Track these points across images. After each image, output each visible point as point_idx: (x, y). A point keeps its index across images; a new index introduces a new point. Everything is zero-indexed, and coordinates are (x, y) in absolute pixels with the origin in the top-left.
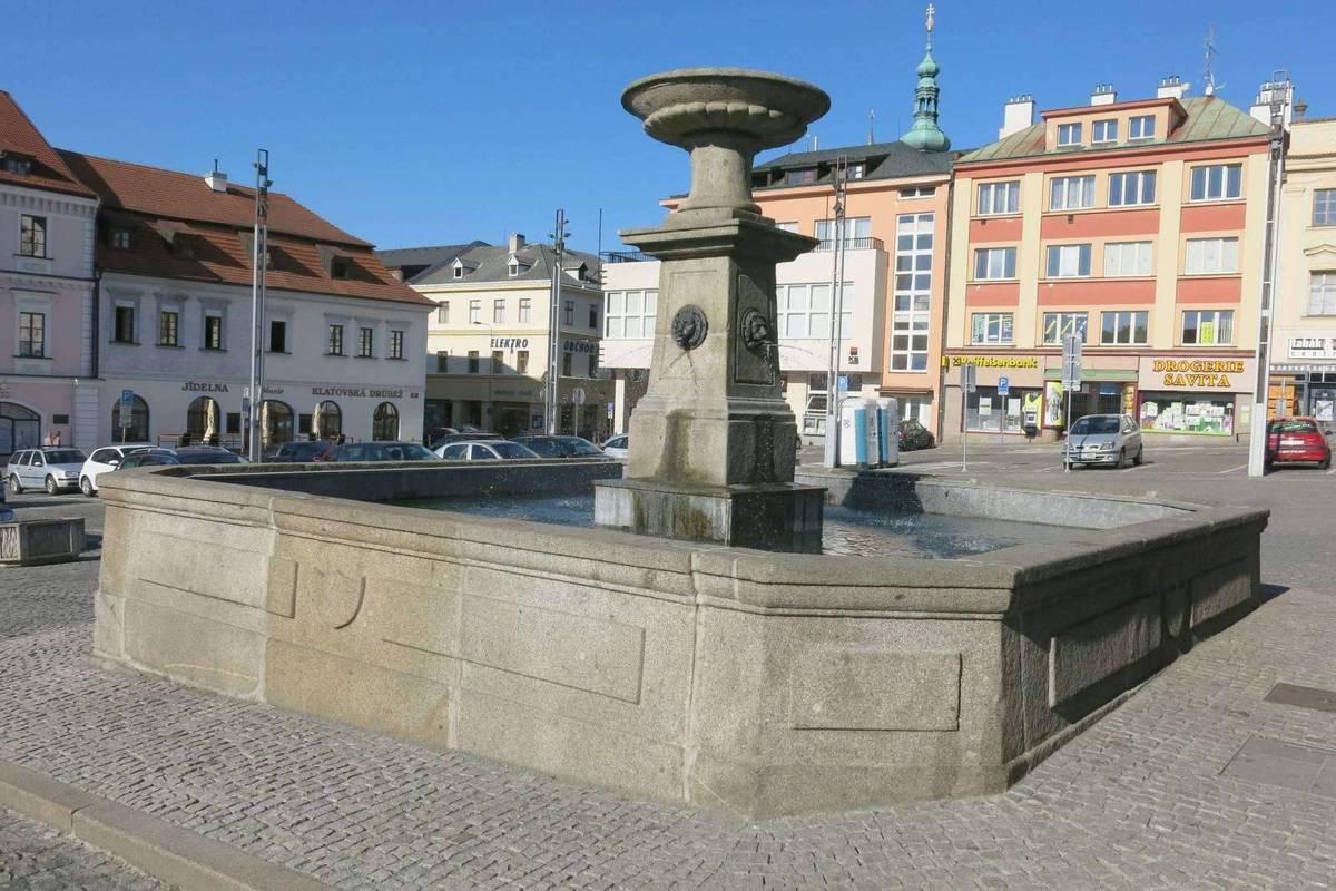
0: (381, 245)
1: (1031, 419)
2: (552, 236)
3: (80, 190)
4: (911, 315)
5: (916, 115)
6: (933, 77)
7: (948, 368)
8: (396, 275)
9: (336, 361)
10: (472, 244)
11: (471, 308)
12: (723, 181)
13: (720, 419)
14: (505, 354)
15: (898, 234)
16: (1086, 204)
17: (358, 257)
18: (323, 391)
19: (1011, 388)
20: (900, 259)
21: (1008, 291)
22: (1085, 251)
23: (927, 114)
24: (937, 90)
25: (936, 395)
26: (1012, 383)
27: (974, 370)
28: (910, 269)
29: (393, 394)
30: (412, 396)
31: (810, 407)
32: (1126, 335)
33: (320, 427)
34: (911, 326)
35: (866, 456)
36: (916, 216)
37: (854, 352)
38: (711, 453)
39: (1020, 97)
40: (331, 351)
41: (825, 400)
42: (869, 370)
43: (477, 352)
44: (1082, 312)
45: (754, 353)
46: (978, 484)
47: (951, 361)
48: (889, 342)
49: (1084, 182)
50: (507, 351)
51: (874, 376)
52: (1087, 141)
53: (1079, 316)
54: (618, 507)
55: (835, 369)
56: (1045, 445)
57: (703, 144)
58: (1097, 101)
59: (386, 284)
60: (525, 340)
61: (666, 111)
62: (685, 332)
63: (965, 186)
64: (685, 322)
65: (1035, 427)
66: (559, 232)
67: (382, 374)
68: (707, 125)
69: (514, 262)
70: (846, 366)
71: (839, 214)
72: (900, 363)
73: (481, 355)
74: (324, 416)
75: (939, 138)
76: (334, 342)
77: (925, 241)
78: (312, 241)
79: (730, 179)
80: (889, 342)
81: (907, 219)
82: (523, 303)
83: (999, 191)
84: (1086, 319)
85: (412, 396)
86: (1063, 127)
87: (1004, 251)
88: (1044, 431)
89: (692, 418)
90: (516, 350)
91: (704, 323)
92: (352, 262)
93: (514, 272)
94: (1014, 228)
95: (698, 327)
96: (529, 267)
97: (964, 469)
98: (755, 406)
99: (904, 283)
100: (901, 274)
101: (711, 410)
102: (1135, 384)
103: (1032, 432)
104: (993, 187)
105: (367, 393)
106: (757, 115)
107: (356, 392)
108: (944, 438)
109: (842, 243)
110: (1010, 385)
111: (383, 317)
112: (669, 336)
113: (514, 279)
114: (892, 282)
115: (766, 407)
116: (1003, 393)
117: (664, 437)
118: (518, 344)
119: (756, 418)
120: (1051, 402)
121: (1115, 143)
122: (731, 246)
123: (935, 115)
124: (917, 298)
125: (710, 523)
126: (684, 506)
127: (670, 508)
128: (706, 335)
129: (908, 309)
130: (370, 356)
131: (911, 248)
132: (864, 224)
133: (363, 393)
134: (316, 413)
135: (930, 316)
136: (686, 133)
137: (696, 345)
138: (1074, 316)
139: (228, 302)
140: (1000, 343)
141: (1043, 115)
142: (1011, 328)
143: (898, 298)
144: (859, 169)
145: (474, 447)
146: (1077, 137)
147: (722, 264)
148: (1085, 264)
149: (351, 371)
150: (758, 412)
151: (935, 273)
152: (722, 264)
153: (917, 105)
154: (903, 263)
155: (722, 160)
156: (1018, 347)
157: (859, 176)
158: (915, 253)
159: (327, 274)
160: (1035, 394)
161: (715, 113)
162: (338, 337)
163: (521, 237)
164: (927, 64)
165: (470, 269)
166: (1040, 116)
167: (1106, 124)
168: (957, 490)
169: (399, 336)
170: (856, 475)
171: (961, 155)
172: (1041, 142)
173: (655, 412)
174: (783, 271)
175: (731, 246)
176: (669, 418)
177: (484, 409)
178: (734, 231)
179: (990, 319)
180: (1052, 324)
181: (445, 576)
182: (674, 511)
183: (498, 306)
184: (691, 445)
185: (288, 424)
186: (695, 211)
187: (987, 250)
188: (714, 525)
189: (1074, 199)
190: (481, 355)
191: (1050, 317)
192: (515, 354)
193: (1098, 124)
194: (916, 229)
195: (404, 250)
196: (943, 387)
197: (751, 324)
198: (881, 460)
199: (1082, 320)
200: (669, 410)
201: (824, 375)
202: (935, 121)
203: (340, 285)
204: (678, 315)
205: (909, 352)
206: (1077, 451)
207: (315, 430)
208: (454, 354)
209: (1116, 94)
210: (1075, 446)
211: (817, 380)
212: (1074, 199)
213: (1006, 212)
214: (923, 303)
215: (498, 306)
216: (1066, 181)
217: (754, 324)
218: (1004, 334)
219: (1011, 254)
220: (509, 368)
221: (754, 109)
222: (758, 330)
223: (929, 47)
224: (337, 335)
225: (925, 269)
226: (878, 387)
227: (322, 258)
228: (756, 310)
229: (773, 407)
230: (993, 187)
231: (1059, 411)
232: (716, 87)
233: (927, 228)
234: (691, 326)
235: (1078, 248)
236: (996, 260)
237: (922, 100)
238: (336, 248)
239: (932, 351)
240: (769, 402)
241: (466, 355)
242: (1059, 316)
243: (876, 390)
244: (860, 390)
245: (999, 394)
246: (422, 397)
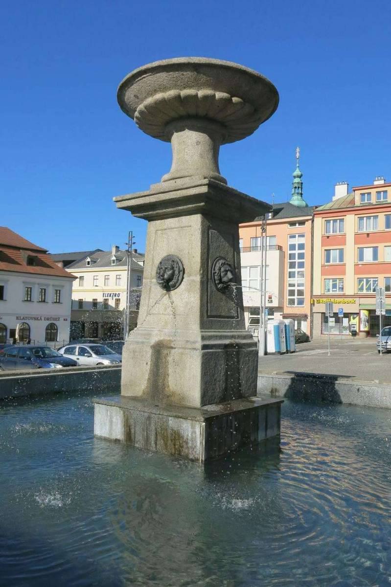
0: (52, 251)
1: (354, 327)
2: (127, 244)
3: (11, 251)
4: (296, 280)
5: (293, 194)
6: (300, 178)
7: (314, 304)
8: (60, 265)
9: (27, 303)
10: (96, 251)
11: (94, 279)
12: (196, 158)
13: (195, 349)
14: (109, 300)
15: (289, 243)
16: (374, 229)
17: (39, 256)
18: (22, 318)
20: (290, 254)
21: (341, 269)
22: (375, 250)
23: (298, 193)
24: (302, 183)
25: (309, 318)
26: (345, 311)
27: (332, 305)
28: (295, 259)
29: (56, 319)
30: (64, 320)
31: (250, 323)
33: (19, 336)
34: (296, 285)
35: (280, 348)
36: (297, 235)
37: (270, 298)
38: (187, 378)
39: (343, 182)
40: (26, 299)
41: (259, 320)
42: (277, 306)
43: (97, 299)
44: (375, 278)
45: (224, 293)
46: (379, 383)
47: (316, 301)
48: (286, 293)
49: (373, 219)
50: (110, 298)
51: (280, 309)
52: (374, 200)
53: (374, 279)
54: (111, 422)
55: (263, 305)
56: (361, 340)
57: (182, 129)
58: (376, 183)
59: (53, 268)
60: (119, 294)
61: (150, 100)
62: (166, 276)
63: (319, 221)
64: (166, 268)
65: (356, 331)
66: (130, 241)
67: (49, 309)
68: (182, 111)
69: (114, 258)
70: (268, 305)
71: (264, 231)
72: (292, 302)
73: (98, 301)
74: (21, 330)
75: (304, 204)
76: (28, 295)
77: (301, 246)
78: (18, 249)
79: (201, 156)
80: (286, 293)
81: (293, 237)
82: (118, 277)
83: (335, 224)
84: (377, 281)
85: (64, 320)
86: (363, 194)
87: (338, 250)
88: (360, 333)
89: (172, 348)
90: (114, 298)
91: (181, 268)
92: (36, 258)
93: (114, 263)
94: (342, 240)
95: (177, 272)
96: (121, 260)
97: (329, 355)
98: (225, 336)
99: (292, 265)
100: (291, 261)
101: (187, 341)
103: (354, 334)
104: (332, 221)
105: (43, 318)
106: (221, 99)
107: (37, 318)
108: (314, 337)
109: (264, 248)
110: (344, 312)
111: (51, 284)
112: (154, 280)
113: (114, 266)
114: (287, 265)
115: (233, 337)
116: (341, 316)
117: (149, 363)
118: (115, 295)
119: (226, 346)
120: (363, 319)
121: (387, 201)
122: (202, 204)
123: (301, 194)
124: (298, 272)
125: (187, 443)
126: (165, 429)
127: (153, 427)
128: (183, 278)
129: (294, 277)
130: (30, 301)
131: (295, 250)
132: (273, 239)
133: (41, 318)
134: (17, 328)
135: (305, 280)
136: (163, 122)
137: (175, 287)
138: (372, 279)
139: (8, 281)
140: (338, 292)
141: (353, 189)
142: (343, 286)
143: (290, 273)
144: (270, 214)
145: (79, 348)
146: (369, 199)
147: (196, 220)
148: (375, 256)
149: (35, 308)
150: (227, 342)
151: (307, 260)
152: (196, 220)
153: (293, 190)
154: (292, 256)
155: (195, 140)
156: (346, 294)
157: (270, 217)
158: (297, 252)
159: (25, 263)
160: (355, 316)
161: (188, 98)
162: (29, 293)
163: (117, 247)
164: (297, 172)
165: (94, 262)
166: (352, 190)
167: (382, 193)
168: (366, 388)
169: (58, 292)
170: (293, 376)
171: (316, 207)
172: (353, 201)
173: (143, 343)
174: (246, 233)
175: (202, 204)
176: (153, 347)
177: (100, 325)
178: (204, 189)
179: (333, 281)
182: (156, 429)
183: (107, 278)
184: (170, 371)
185: (4, 334)
186: (174, 181)
187: (330, 250)
188: (190, 445)
189: (369, 226)
190: (98, 301)
191: (360, 280)
192: (114, 300)
193: (378, 193)
194: (297, 241)
195: (65, 254)
196: (312, 314)
197: (220, 269)
198: (287, 350)
199: (375, 281)
200: (154, 340)
201: (259, 308)
202: (301, 196)
203: (31, 269)
204: (161, 263)
205: (296, 297)
206: (385, 344)
207: (17, 336)
208: (86, 300)
209: (385, 180)
210: (383, 342)
211: (255, 311)
212: (369, 226)
213: (338, 233)
214: (302, 275)
215: (107, 278)
216: (365, 218)
217: (222, 269)
218: (339, 288)
219: (341, 252)
220: (111, 307)
221: (219, 95)
222: (226, 274)
223: (298, 165)
224: (29, 292)
225: (301, 259)
226: (282, 313)
227: (23, 256)
228: (221, 258)
229: (239, 337)
230: (332, 221)
231: (367, 324)
232: (188, 74)
233: (302, 241)
234: (170, 272)
235: (372, 248)
236: (335, 254)
237: (296, 187)
238: (30, 252)
239: (307, 297)
240: (235, 333)
241: (92, 301)
242: (365, 280)
243: (281, 315)
245: (339, 316)
246: (69, 320)
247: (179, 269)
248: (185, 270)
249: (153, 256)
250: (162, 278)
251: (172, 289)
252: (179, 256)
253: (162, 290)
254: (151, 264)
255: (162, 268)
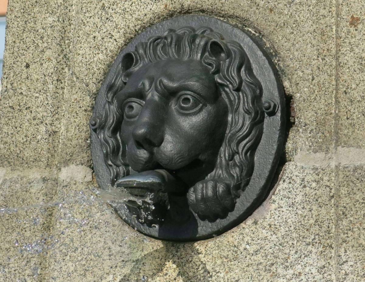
62: (170, 146)
64: (169, 95)
91: (270, 94)
95: (239, 121)
112: (76, 173)
128: (281, 159)
137: (226, 213)
204: (128, 60)
247: (257, 98)
248: (297, 105)
249: (65, 20)
250: (143, 154)
251: (204, 227)
252: (255, 17)
253: (130, 234)
254: (50, 67)
255: (141, 95)
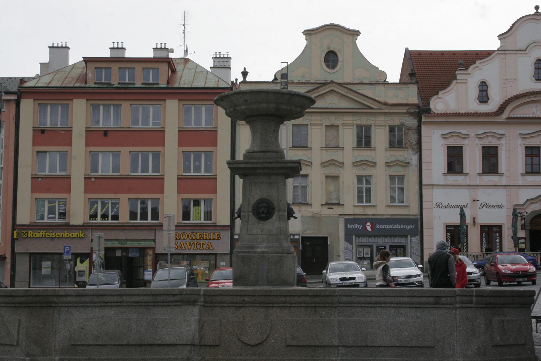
19: (72, 254)
32: (148, 216)
102: (154, 249)
112: (251, 214)
180: (106, 207)
181: (323, 313)
186: (264, 153)
196: (14, 254)
244: (522, 229)
